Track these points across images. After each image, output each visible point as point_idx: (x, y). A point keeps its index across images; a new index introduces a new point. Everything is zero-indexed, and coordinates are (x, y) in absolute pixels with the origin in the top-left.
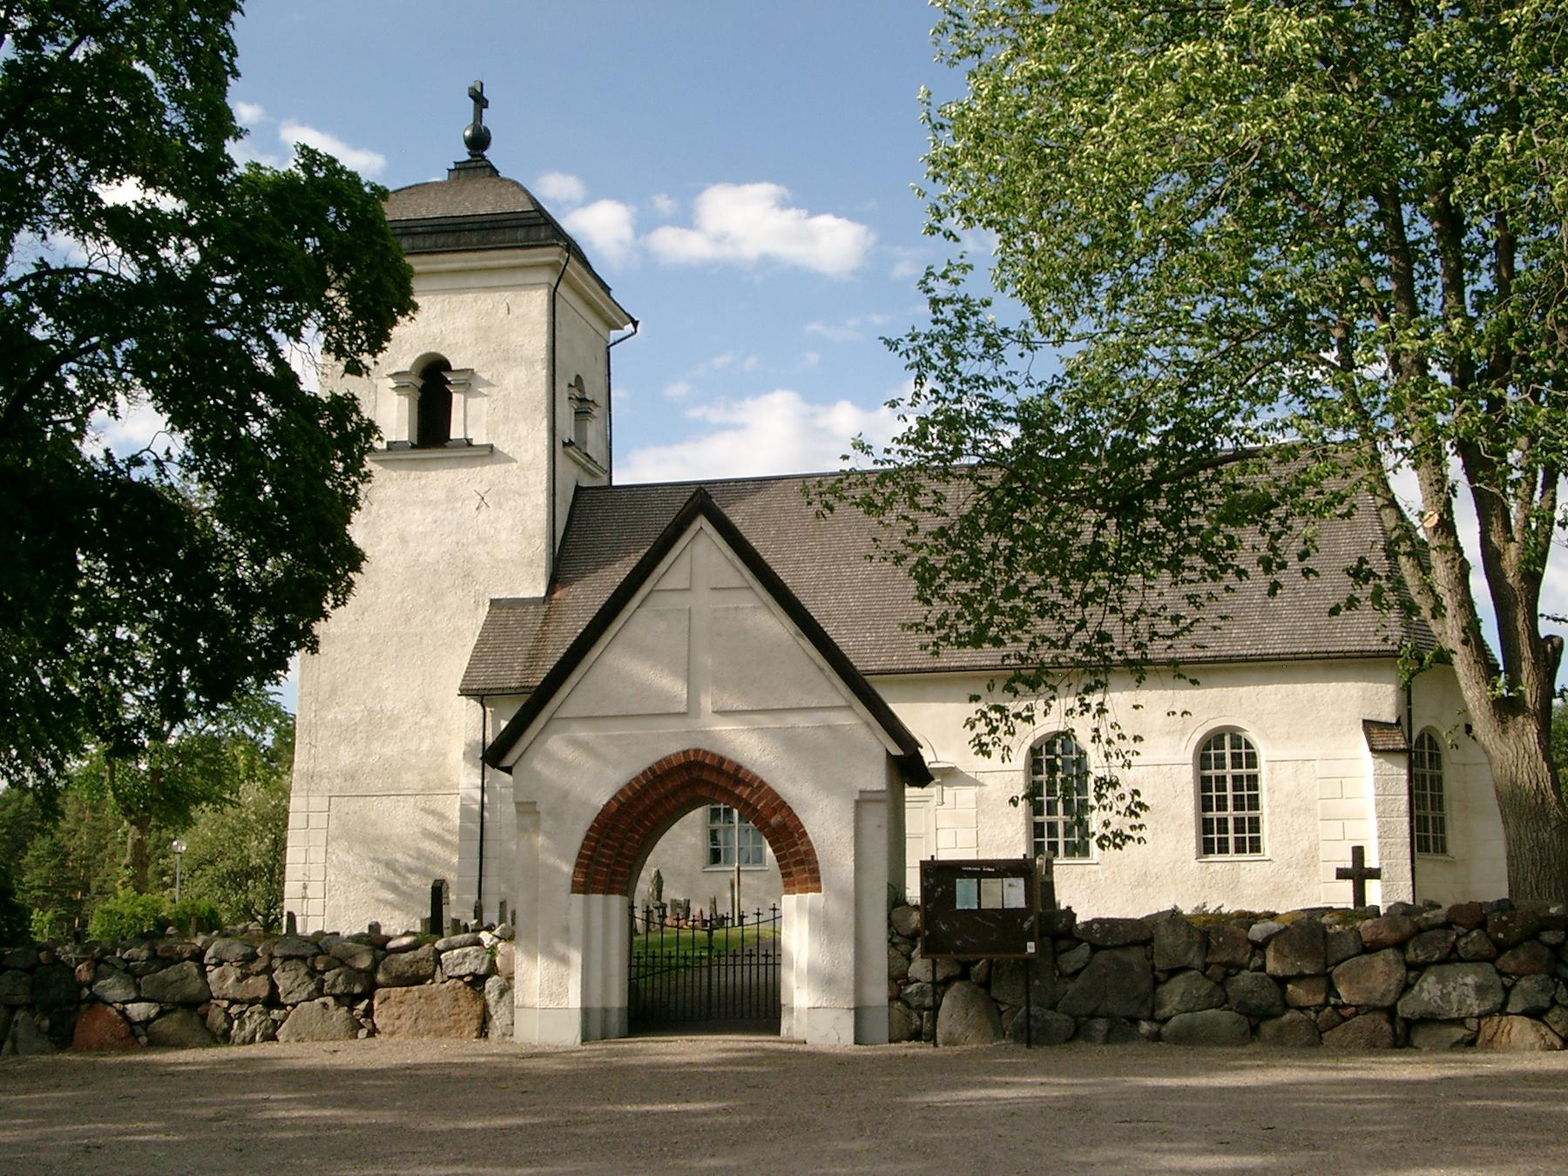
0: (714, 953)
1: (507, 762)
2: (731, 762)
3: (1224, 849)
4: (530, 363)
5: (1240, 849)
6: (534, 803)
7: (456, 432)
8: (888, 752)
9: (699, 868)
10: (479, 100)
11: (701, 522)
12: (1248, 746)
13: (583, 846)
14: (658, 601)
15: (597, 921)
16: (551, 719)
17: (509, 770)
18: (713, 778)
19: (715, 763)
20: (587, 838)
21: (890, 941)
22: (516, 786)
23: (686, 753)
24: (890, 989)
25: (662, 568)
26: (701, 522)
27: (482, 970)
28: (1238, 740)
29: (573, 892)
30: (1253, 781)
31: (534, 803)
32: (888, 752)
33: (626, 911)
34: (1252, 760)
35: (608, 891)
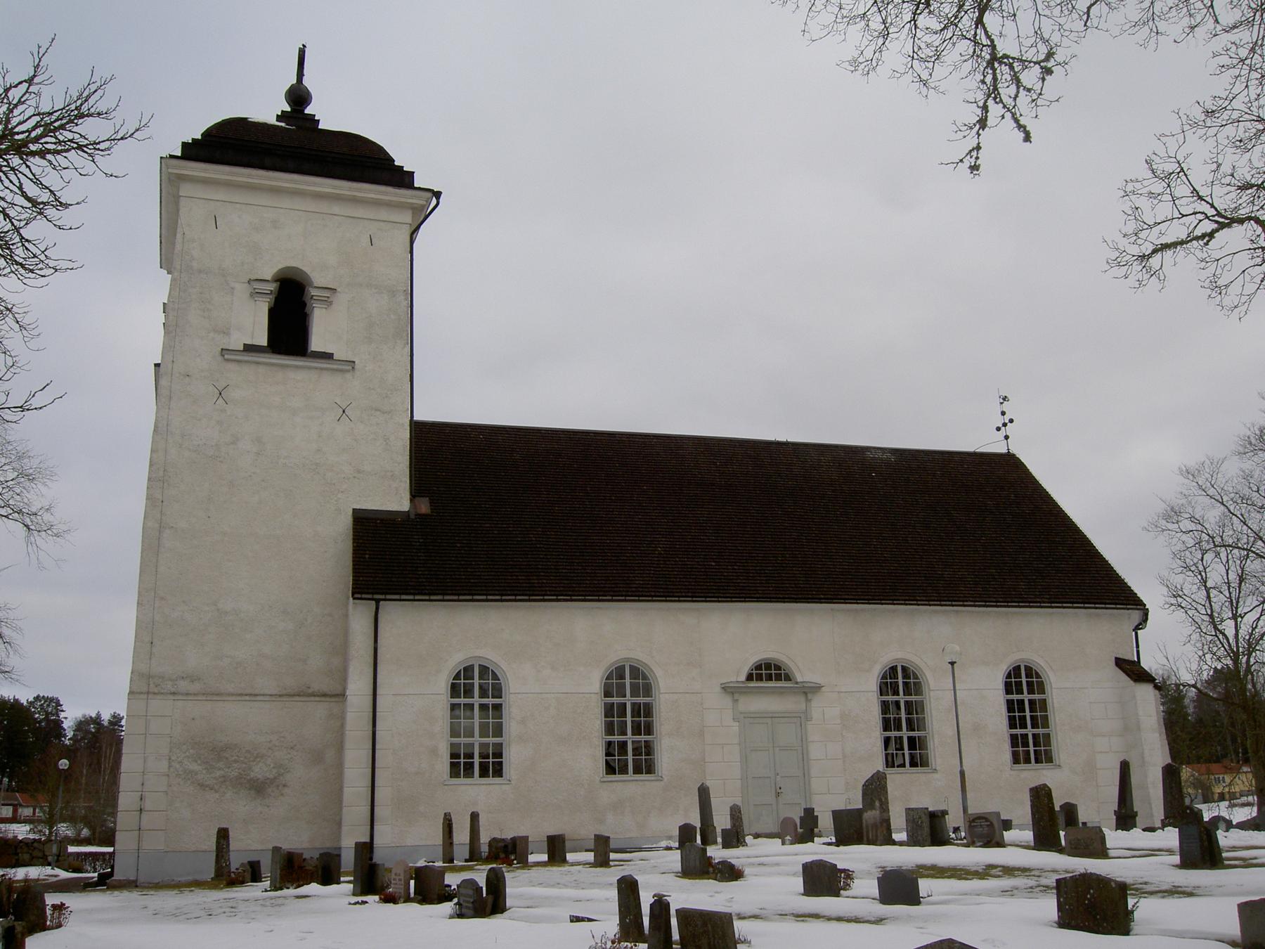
4: (393, 293)
7: (316, 344)
9: (598, 779)
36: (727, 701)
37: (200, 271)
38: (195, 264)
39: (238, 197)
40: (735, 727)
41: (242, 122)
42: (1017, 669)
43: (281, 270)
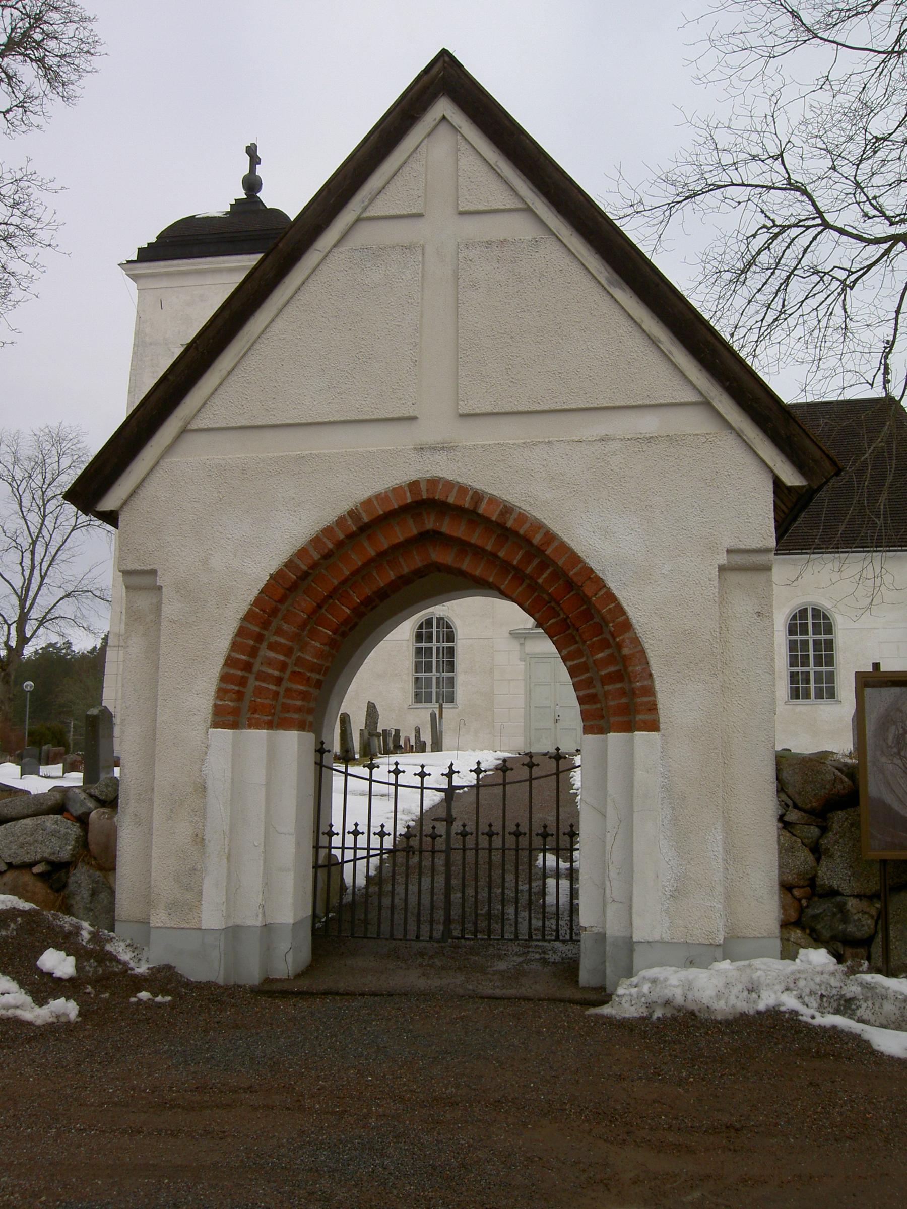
0: (457, 827)
1: (108, 503)
2: (493, 500)
3: (807, 696)
5: (819, 695)
6: (153, 572)
8: (778, 484)
10: (255, 160)
11: (443, 107)
12: (826, 617)
13: (234, 646)
14: (366, 235)
15: (257, 775)
16: (184, 431)
17: (111, 518)
18: (459, 531)
19: (467, 503)
20: (241, 632)
21: (781, 819)
22: (124, 549)
23: (414, 485)
24: (784, 907)
25: (375, 181)
26: (443, 107)
27: (65, 853)
28: (817, 613)
29: (216, 725)
30: (829, 645)
31: (153, 572)
32: (778, 484)
33: (311, 758)
34: (829, 629)
35: (276, 722)
36: (515, 645)
37: (151, 344)
38: (147, 339)
39: (176, 282)
40: (522, 666)
41: (189, 222)
42: (803, 612)
43: (433, 482)
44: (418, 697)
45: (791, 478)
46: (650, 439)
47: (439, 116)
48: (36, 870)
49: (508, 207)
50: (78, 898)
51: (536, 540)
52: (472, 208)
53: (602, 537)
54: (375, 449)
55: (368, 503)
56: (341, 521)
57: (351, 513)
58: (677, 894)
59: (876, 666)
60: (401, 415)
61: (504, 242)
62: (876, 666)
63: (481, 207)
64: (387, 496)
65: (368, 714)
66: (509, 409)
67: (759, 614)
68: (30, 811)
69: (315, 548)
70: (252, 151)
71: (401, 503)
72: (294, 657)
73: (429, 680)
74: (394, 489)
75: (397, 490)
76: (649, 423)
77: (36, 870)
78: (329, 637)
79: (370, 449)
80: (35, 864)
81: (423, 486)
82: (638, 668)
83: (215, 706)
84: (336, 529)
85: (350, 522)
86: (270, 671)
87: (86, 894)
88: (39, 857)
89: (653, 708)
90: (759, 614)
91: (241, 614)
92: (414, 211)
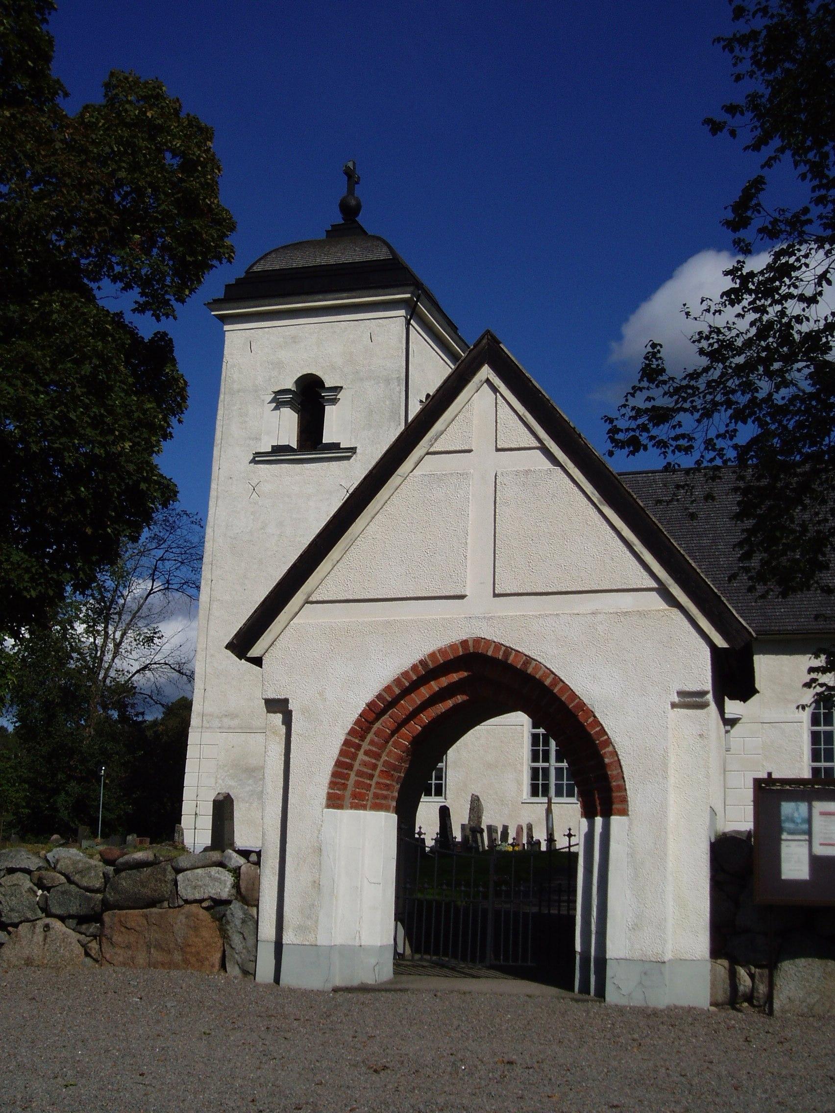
1: (254, 652)
17: (258, 662)
23: (464, 643)
31: (286, 701)
43: (478, 641)
44: (535, 792)
45: (720, 642)
46: (626, 614)
47: (484, 379)
48: (205, 904)
49: (532, 446)
50: (232, 925)
51: (547, 682)
52: (506, 446)
53: (590, 681)
54: (438, 617)
55: (432, 655)
56: (414, 668)
57: (421, 662)
58: (635, 928)
59: (770, 774)
60: (456, 594)
61: (527, 472)
62: (770, 774)
63: (513, 446)
64: (446, 651)
65: (472, 809)
66: (529, 591)
67: (701, 736)
68: (200, 864)
69: (397, 686)
70: (349, 174)
71: (456, 655)
72: (382, 760)
73: (546, 771)
74: (451, 645)
75: (452, 647)
76: (627, 601)
77: (205, 904)
78: (407, 746)
79: (434, 617)
80: (203, 900)
81: (471, 643)
82: (615, 773)
83: (328, 793)
84: (411, 673)
85: (420, 668)
86: (365, 770)
87: (238, 922)
88: (206, 896)
89: (624, 800)
90: (701, 736)
91: (347, 731)
92: (466, 448)
